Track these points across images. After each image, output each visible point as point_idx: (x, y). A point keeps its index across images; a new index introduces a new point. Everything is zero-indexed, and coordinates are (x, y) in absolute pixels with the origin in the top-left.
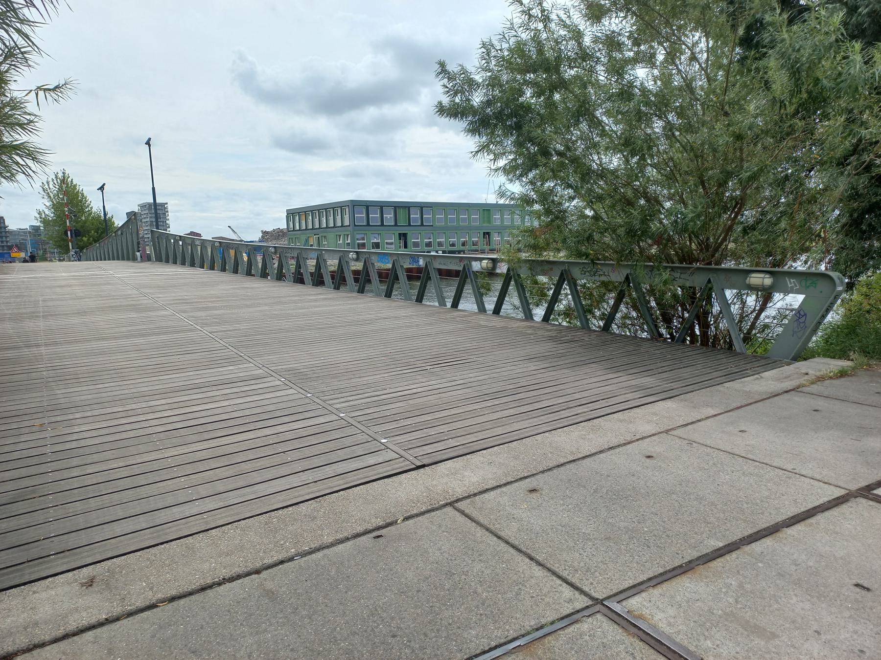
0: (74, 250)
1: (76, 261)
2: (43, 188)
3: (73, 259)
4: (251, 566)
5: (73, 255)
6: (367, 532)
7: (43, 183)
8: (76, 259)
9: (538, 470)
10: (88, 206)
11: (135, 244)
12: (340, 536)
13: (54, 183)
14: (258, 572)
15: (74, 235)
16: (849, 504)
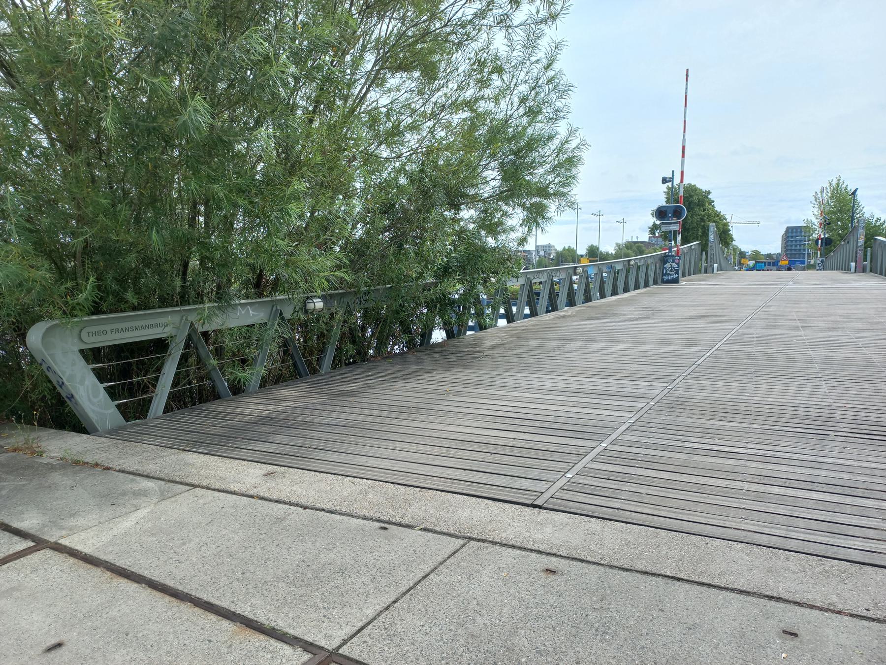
0: (821, 259)
1: (821, 270)
2: (815, 198)
3: (818, 268)
4: (303, 501)
5: (818, 264)
6: (379, 520)
7: (816, 192)
8: (821, 267)
9: (561, 550)
10: (860, 213)
11: (854, 252)
12: (524, 553)
13: (828, 192)
14: (305, 508)
15: (824, 244)
16: (61, 555)
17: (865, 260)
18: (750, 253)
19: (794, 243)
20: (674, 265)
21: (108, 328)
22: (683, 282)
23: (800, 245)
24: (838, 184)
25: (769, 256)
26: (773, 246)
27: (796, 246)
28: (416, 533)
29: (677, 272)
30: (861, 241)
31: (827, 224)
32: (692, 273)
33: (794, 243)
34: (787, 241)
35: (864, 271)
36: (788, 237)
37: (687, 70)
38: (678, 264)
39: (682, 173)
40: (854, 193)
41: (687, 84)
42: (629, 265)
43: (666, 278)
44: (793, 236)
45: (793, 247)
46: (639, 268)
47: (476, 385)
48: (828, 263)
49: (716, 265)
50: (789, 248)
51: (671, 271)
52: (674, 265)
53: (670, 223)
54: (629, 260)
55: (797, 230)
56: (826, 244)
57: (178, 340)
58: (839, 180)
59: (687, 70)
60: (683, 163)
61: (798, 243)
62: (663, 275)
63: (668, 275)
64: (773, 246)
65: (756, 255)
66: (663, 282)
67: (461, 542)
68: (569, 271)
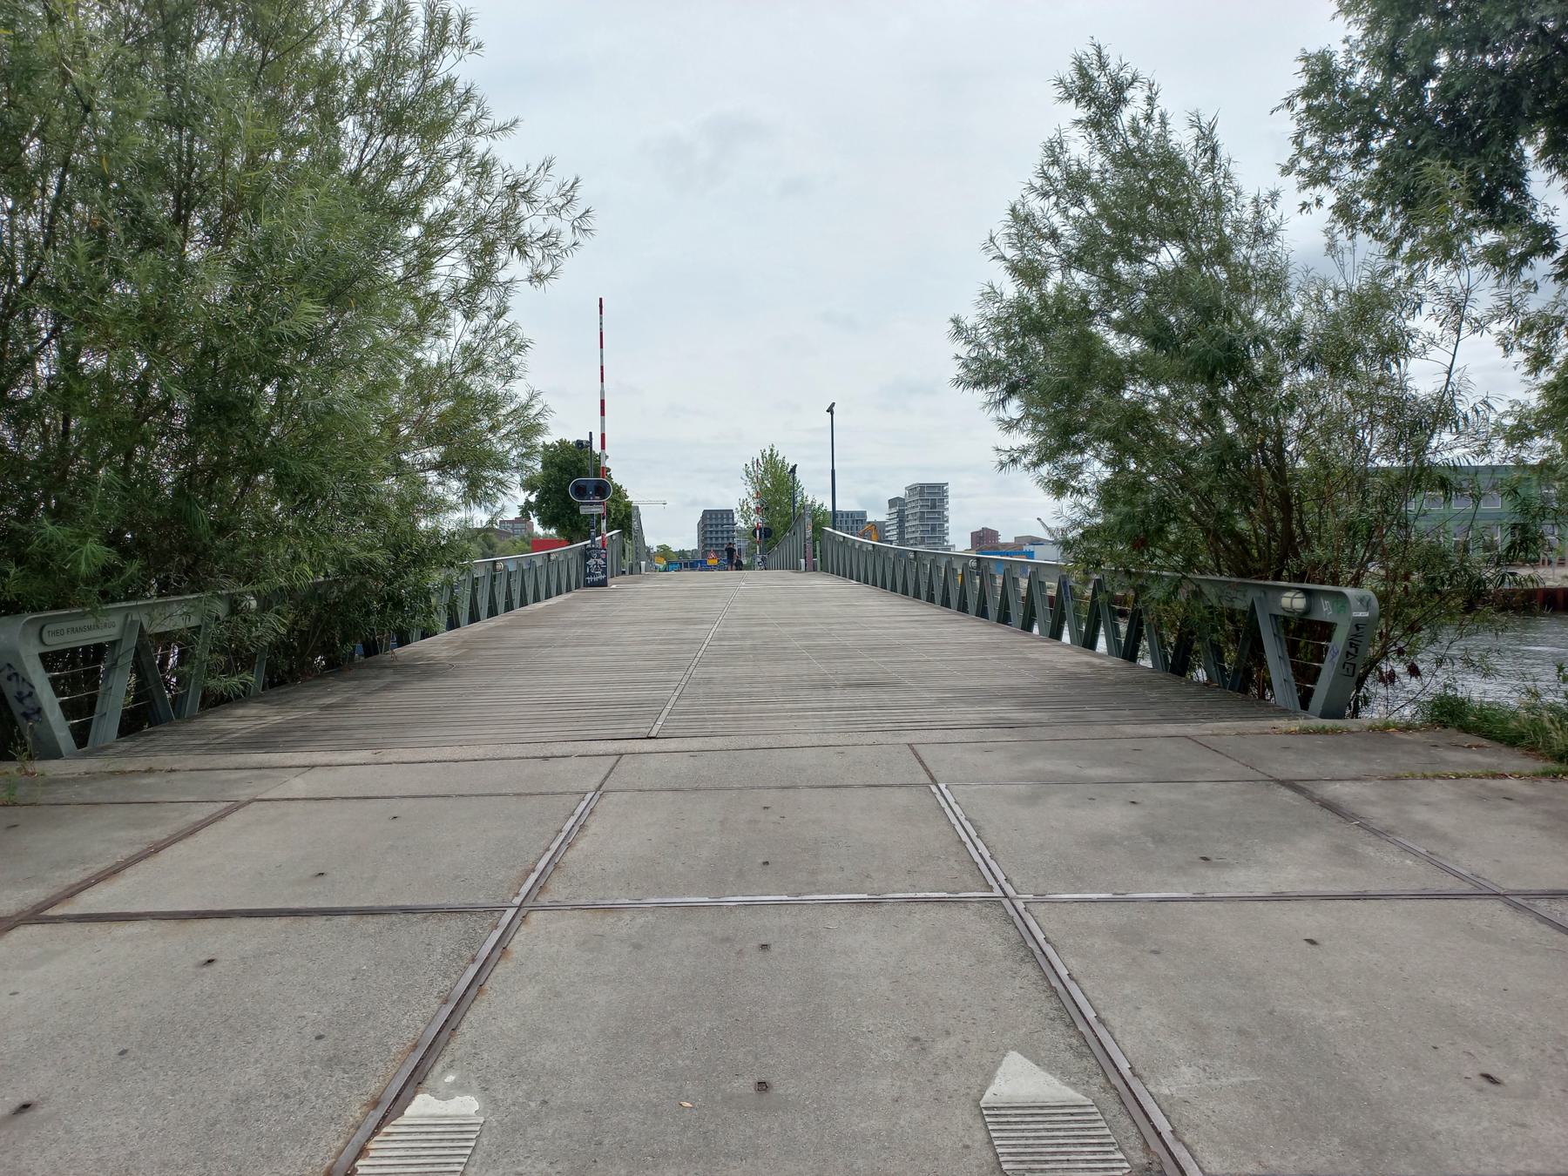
17: (815, 556)
18: (655, 550)
19: (714, 535)
20: (600, 561)
21: (65, 626)
22: (613, 584)
23: (728, 538)
24: (771, 455)
25: (682, 553)
26: (686, 539)
27: (723, 538)
28: (573, 760)
29: (605, 571)
30: (809, 532)
31: (763, 509)
32: (573, 586)
33: (714, 535)
34: (706, 532)
35: (815, 569)
36: (706, 525)
37: (601, 299)
38: (605, 560)
39: (603, 436)
40: (793, 470)
41: (601, 318)
42: (495, 569)
43: (590, 579)
44: (714, 523)
45: (714, 541)
46: (510, 574)
47: (488, 687)
48: (772, 561)
49: (643, 563)
50: (709, 541)
51: (597, 569)
52: (600, 561)
53: (592, 504)
54: (495, 562)
55: (717, 515)
56: (765, 536)
57: (124, 646)
58: (772, 450)
59: (601, 299)
60: (603, 422)
61: (720, 535)
62: (587, 575)
63: (593, 575)
64: (686, 539)
65: (664, 551)
66: (587, 585)
67: (616, 758)
68: (135, 617)
